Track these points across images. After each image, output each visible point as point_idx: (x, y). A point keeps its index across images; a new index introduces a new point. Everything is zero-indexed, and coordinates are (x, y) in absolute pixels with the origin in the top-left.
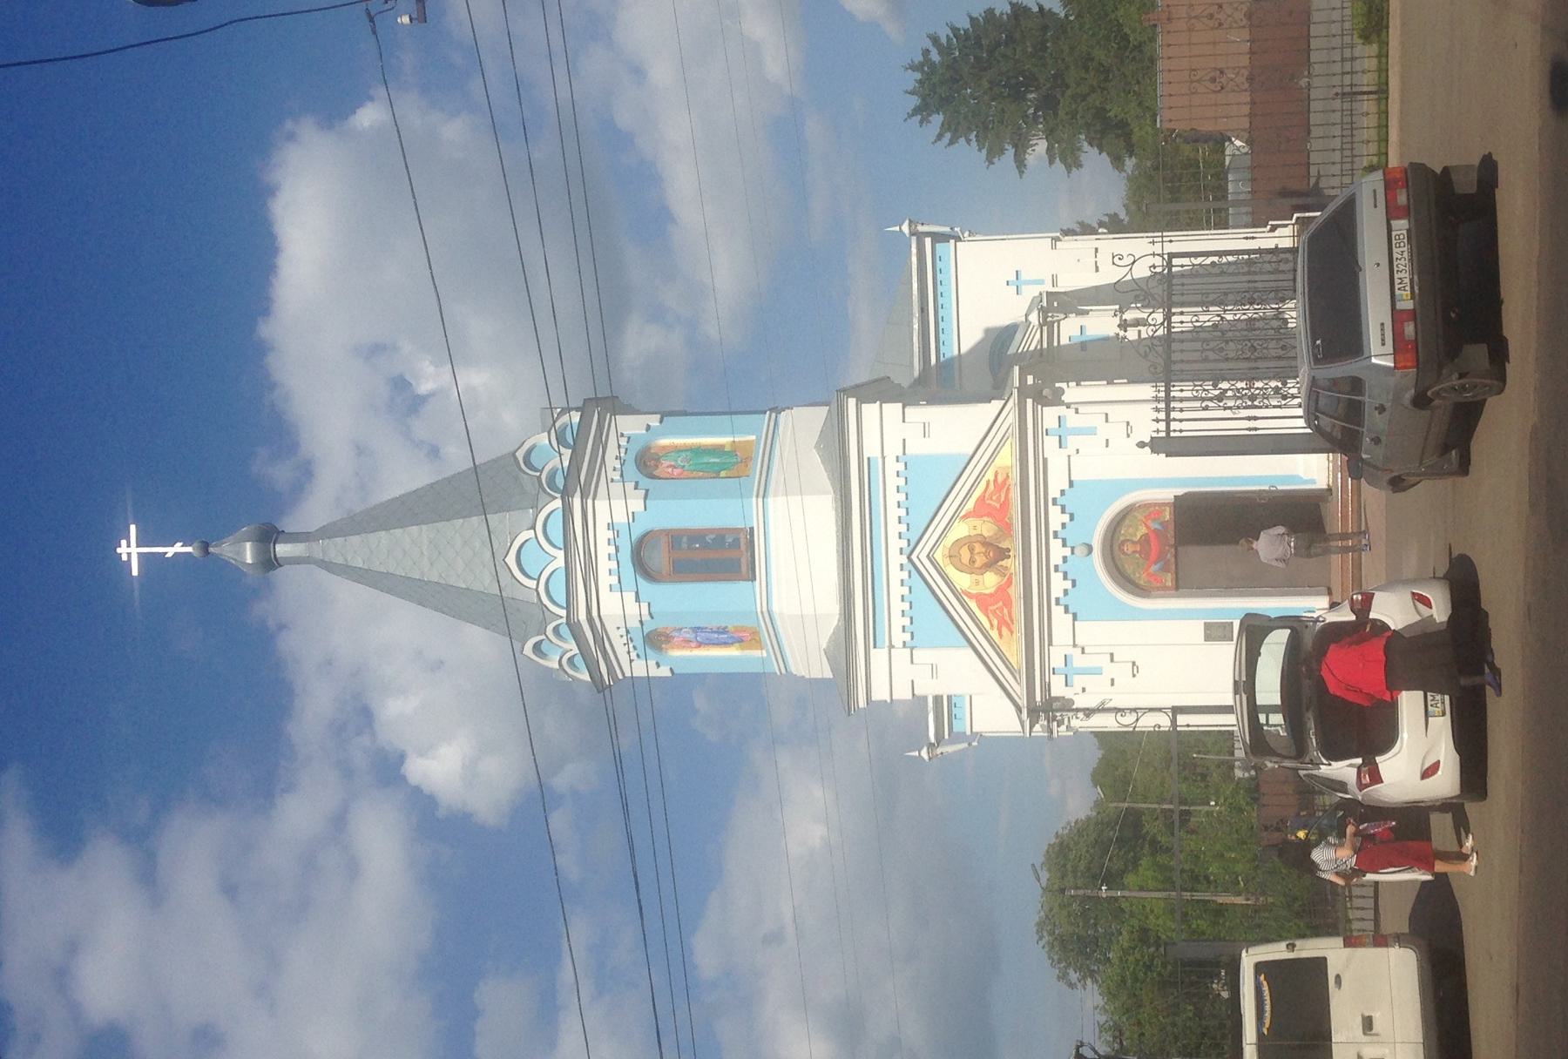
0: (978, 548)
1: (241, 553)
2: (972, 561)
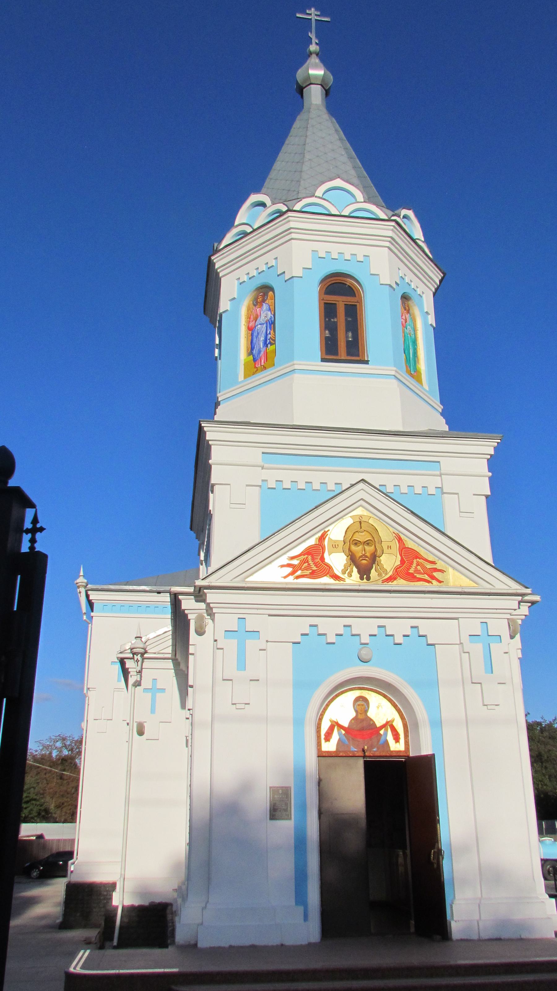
0: (369, 549)
1: (316, 67)
2: (356, 543)
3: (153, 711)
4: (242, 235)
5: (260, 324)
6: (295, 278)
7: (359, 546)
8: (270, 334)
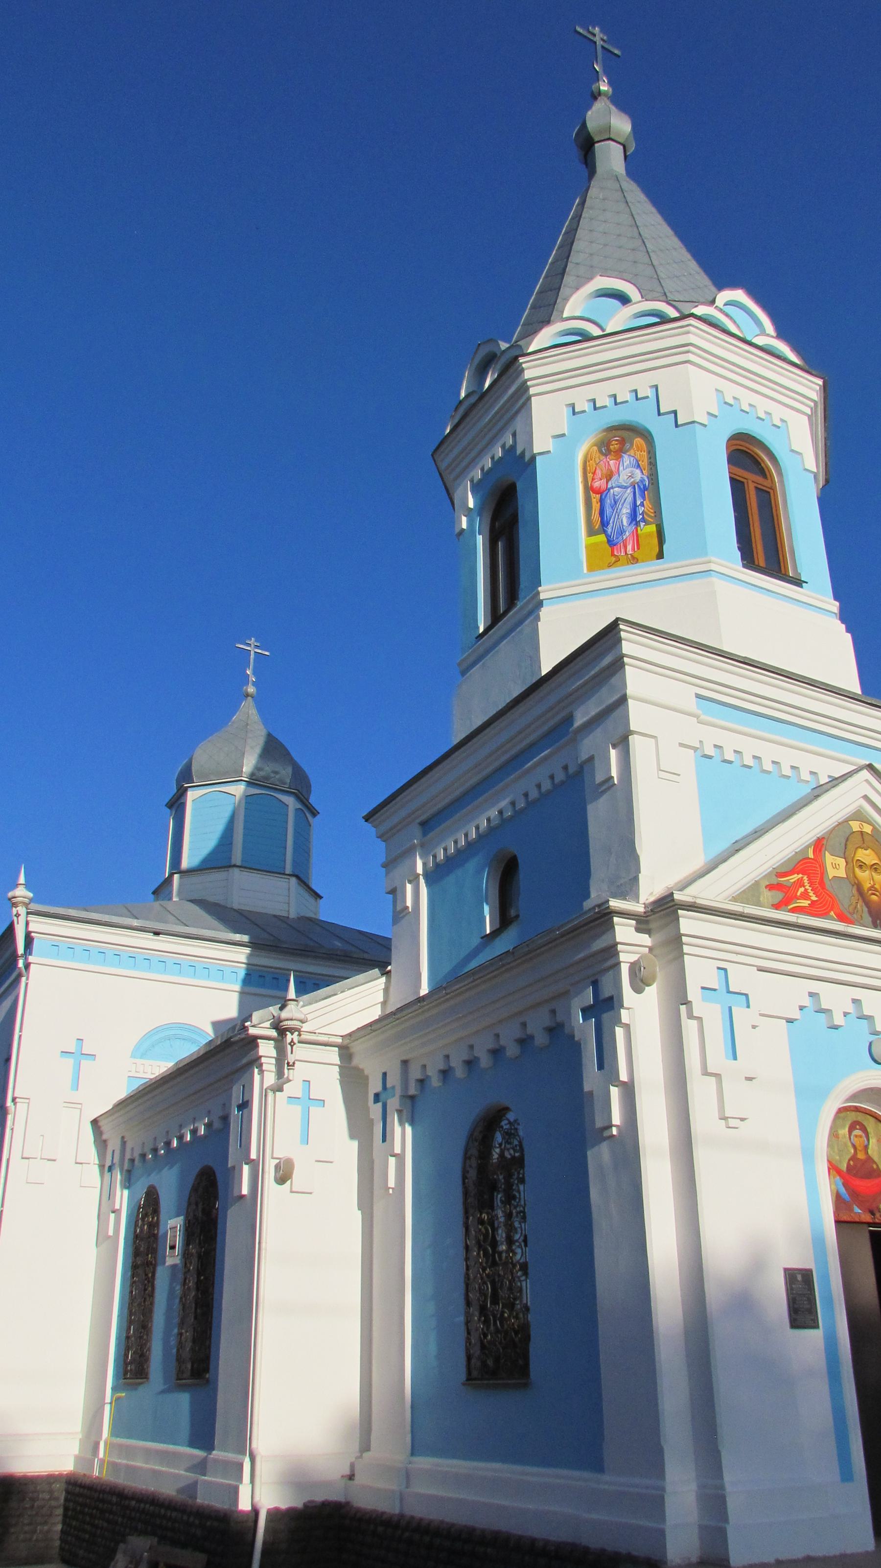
3: (306, 1139)
4: (579, 338)
5: (619, 487)
6: (696, 424)
7: (866, 871)
8: (642, 504)
